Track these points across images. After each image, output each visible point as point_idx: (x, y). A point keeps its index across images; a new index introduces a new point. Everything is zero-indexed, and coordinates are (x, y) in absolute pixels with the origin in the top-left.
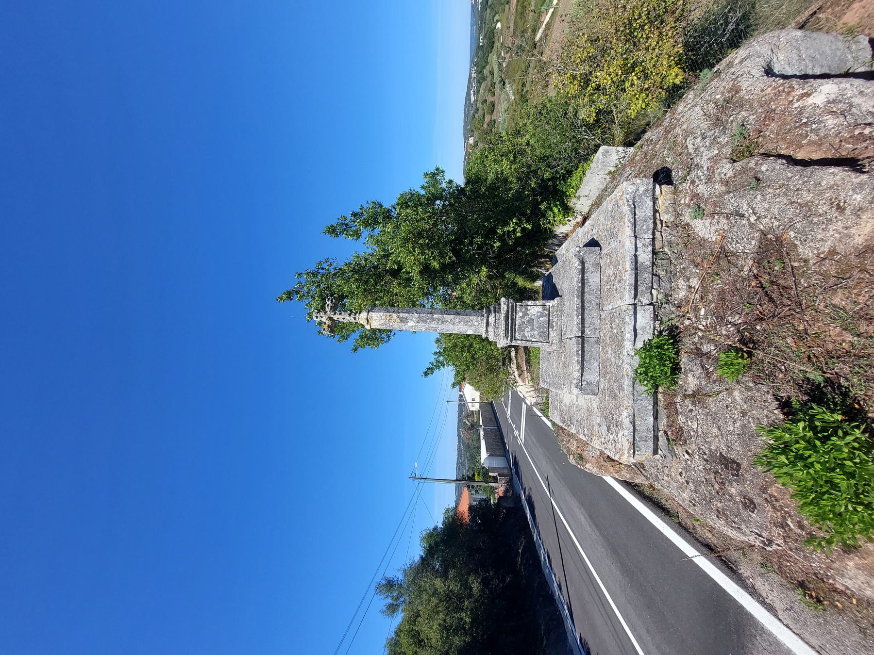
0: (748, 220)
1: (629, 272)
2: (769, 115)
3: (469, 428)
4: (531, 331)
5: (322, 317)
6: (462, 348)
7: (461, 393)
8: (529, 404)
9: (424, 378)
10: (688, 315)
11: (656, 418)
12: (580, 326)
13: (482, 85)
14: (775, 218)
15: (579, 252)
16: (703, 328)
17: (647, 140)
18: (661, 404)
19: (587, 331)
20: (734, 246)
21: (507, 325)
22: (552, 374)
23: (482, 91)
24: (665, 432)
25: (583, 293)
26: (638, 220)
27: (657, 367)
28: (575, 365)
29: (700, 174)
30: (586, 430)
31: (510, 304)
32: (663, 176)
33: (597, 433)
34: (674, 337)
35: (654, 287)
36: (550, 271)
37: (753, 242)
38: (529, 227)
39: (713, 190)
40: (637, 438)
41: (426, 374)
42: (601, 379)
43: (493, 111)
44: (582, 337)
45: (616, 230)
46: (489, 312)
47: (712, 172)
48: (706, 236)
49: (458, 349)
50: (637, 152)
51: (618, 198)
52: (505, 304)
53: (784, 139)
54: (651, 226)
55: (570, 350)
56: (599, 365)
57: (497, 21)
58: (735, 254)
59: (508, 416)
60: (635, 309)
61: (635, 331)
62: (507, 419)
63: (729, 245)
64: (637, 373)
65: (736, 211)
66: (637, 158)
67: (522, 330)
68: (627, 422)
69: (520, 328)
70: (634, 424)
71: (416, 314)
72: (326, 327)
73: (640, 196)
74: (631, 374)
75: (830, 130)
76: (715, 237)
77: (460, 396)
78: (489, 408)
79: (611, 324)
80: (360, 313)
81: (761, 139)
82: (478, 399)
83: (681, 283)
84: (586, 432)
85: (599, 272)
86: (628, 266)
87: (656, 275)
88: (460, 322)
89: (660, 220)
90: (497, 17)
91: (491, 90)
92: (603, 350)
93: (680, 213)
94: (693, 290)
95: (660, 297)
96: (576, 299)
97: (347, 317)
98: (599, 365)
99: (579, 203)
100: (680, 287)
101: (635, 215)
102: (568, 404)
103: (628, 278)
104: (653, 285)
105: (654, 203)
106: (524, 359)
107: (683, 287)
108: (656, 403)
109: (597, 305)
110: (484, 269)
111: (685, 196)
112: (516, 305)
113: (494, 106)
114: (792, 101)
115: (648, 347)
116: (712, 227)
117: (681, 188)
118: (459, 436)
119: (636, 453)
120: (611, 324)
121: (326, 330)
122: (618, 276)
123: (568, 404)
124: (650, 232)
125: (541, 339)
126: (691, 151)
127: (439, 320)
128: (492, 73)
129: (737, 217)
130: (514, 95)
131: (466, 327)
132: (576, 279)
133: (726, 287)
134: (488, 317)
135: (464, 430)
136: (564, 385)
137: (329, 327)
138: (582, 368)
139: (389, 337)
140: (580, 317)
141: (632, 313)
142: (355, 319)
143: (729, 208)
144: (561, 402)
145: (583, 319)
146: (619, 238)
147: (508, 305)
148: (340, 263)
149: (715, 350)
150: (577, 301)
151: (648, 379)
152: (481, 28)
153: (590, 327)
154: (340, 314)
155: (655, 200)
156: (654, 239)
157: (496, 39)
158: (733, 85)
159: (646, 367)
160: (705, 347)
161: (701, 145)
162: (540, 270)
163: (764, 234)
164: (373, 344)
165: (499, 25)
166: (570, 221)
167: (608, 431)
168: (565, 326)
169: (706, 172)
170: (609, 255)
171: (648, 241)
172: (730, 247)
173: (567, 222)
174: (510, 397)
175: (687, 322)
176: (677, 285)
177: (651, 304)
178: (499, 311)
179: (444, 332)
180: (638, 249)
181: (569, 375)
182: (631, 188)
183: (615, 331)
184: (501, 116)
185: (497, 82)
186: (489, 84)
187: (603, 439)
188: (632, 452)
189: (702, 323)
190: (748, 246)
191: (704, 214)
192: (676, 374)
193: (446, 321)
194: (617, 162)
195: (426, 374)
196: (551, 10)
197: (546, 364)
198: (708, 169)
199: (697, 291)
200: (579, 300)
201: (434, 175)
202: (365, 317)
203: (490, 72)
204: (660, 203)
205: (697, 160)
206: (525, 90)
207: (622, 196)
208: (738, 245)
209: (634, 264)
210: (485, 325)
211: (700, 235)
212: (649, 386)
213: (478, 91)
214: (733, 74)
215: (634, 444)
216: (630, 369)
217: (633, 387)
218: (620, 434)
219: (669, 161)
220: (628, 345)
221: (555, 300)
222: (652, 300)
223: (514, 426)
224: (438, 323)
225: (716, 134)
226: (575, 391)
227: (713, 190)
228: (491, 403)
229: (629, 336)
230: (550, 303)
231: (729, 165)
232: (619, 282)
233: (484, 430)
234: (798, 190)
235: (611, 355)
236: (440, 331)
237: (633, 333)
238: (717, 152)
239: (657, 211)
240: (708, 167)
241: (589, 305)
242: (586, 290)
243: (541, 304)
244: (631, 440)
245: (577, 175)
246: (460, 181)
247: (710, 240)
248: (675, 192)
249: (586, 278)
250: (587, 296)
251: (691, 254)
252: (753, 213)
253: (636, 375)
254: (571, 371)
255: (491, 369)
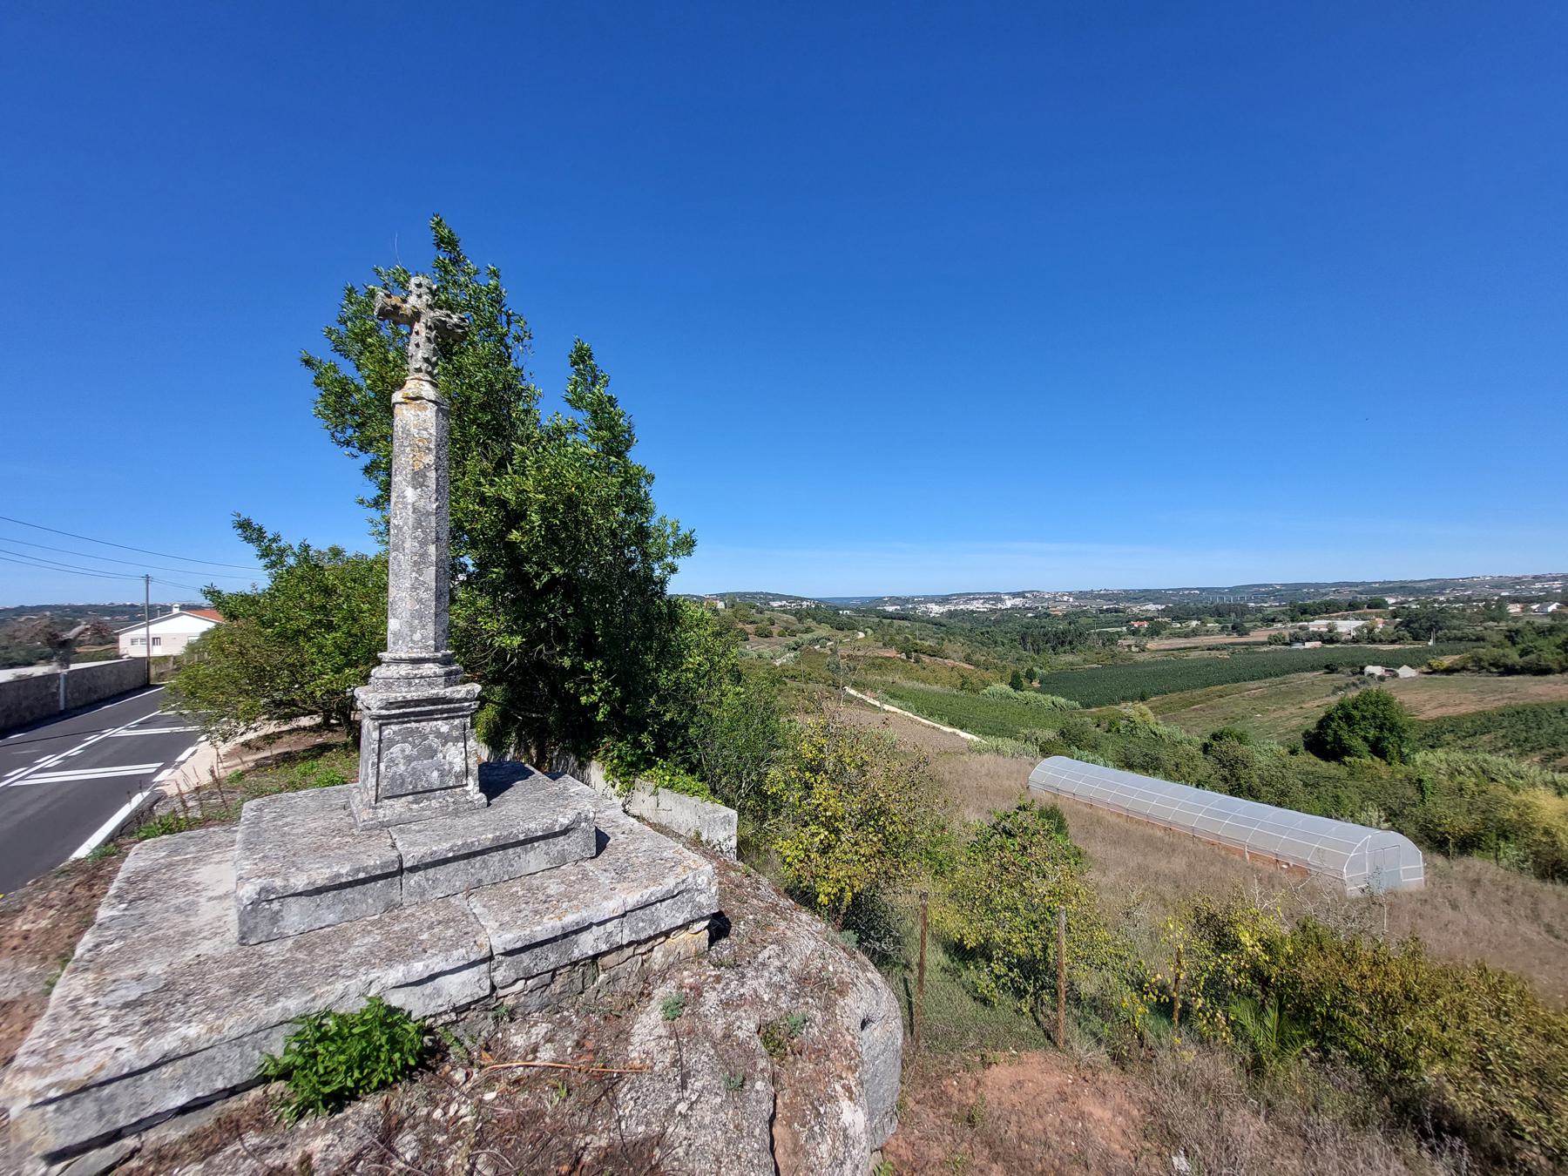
0: (679, 1100)
1: (559, 924)
2: (821, 1054)
3: (56, 636)
4: (405, 758)
5: (419, 296)
6: (323, 607)
7: (176, 611)
8: (157, 779)
9: (230, 520)
10: (475, 1070)
11: (183, 1110)
12: (429, 860)
13: (794, 618)
14: (690, 1145)
15: (587, 819)
16: (452, 1112)
17: (757, 882)
18: (233, 1103)
19: (414, 880)
20: (629, 1096)
21: (418, 703)
22: (286, 825)
23: (786, 617)
24: (134, 1152)
25: (504, 847)
26: (653, 909)
27: (342, 1058)
28: (327, 873)
29: (733, 985)
30: (116, 946)
31: (467, 704)
32: (719, 927)
33: (110, 978)
34: (421, 1063)
35: (529, 982)
36: (536, 772)
37: (641, 1129)
38: (600, 717)
39: (713, 1018)
40: (107, 1090)
41: (244, 525)
42: (290, 943)
43: (760, 635)
44: (401, 871)
45: (632, 876)
46: (446, 661)
47: (738, 1005)
48: (635, 1040)
49: (318, 600)
50: (740, 871)
51: (685, 863)
52: (468, 692)
53: (796, 1094)
54: (643, 936)
55: (365, 852)
56: (328, 926)
57: (866, 633)
58: (612, 1105)
59: (109, 733)
60: (483, 961)
61: (432, 978)
62: (98, 731)
63: (628, 1086)
64: (322, 1018)
65: (689, 1072)
66: (733, 874)
67: (406, 736)
68: (168, 1042)
69: (412, 732)
70: (166, 1060)
71: (434, 506)
72: (395, 300)
73: (692, 900)
74: (319, 1005)
75: (815, 1155)
76: (636, 1055)
77: (169, 609)
78: (130, 680)
79: (440, 923)
80: (431, 383)
81: (791, 1059)
82: (157, 651)
83: (542, 1029)
84: (106, 949)
85: (549, 866)
86: (570, 919)
87: (553, 976)
88: (420, 601)
89: (653, 947)
90: (870, 632)
91: (788, 631)
92: (372, 923)
93: (667, 976)
94: (530, 1057)
95: (510, 1002)
96: (490, 836)
97: (420, 354)
98: (328, 926)
99: (646, 796)
100: (533, 1030)
101: (661, 901)
102: (196, 878)
103: (548, 926)
104: (533, 977)
105: (680, 927)
106: (294, 749)
107: (534, 1037)
108: (232, 1092)
109: (480, 881)
110: (517, 640)
111: (695, 974)
112: (467, 716)
113: (767, 636)
114: (842, 1078)
115: (390, 1018)
116: (653, 1043)
117: (705, 962)
118: (21, 611)
119: (52, 1107)
120: (440, 923)
121: (387, 300)
122: (546, 905)
123: (196, 878)
124: (634, 938)
125: (384, 783)
126: (761, 957)
127: (421, 555)
128: (808, 630)
129: (678, 1079)
130: (781, 665)
131: (406, 615)
132: (533, 825)
133: (547, 1120)
134: (434, 661)
135: (46, 621)
136: (261, 859)
137: (396, 308)
138: (319, 891)
139: (348, 443)
140: (450, 855)
141: (473, 958)
142: (419, 370)
143: (693, 1059)
144: (197, 860)
145: (446, 861)
146: (619, 886)
147: (466, 700)
148: (521, 356)
149: (406, 1162)
150: (487, 838)
151: (306, 1050)
152: (858, 611)
153: (428, 880)
154: (429, 339)
155: (685, 926)
156: (621, 947)
157: (846, 632)
158: (849, 983)
159: (339, 1033)
160: (408, 1138)
161: (772, 969)
162: (512, 750)
163: (660, 1140)
164: (326, 407)
165: (861, 635)
166: (613, 786)
167: (126, 1005)
168: (422, 827)
169: (737, 993)
170: (585, 876)
171: (618, 939)
172: (625, 1090)
173: (610, 782)
174: (181, 729)
175: (459, 1076)
176: (536, 1024)
177: (493, 988)
178: (448, 683)
179: (393, 566)
180: (602, 927)
181: (294, 864)
182: (702, 880)
183: (425, 936)
184: (753, 649)
185: (796, 639)
186: (794, 628)
187: (90, 1000)
188: (53, 1094)
189: (463, 1107)
190: (633, 1122)
191: (673, 1020)
192: (325, 1106)
193: (420, 572)
194: (715, 842)
195: (244, 525)
196: (877, 703)
197: (312, 805)
198: (741, 995)
199: (528, 1066)
200: (488, 844)
201: (687, 545)
202: (424, 394)
203: (809, 628)
204: (681, 936)
205: (750, 973)
206: (787, 680)
207: (690, 868)
208: (632, 1103)
209: (576, 928)
210: (414, 655)
211: (636, 1027)
212: (288, 1059)
213: (785, 612)
214: (857, 977)
215: (85, 1089)
216: (332, 998)
217: (281, 1023)
218: (119, 1041)
219: (739, 928)
220: (397, 974)
221: (481, 795)
222: (502, 988)
223: (75, 751)
224: (415, 554)
225: (789, 987)
226: (249, 891)
227: (713, 1018)
228: (147, 686)
229: (419, 968)
230: (472, 785)
231: (752, 1026)
232: (536, 912)
233: (51, 678)
234: (739, 1157)
235: (362, 944)
236: (395, 558)
237: (426, 975)
238: (766, 1000)
239: (668, 937)
240: (744, 994)
241: (477, 865)
242: (511, 851)
243: (470, 766)
244: (102, 1076)
245: (690, 781)
246: (674, 587)
247: (630, 1048)
248: (699, 955)
249: (536, 844)
250: (497, 856)
251: (599, 1026)
252: (692, 1104)
253: (316, 1018)
254: (307, 866)
255: (260, 677)
